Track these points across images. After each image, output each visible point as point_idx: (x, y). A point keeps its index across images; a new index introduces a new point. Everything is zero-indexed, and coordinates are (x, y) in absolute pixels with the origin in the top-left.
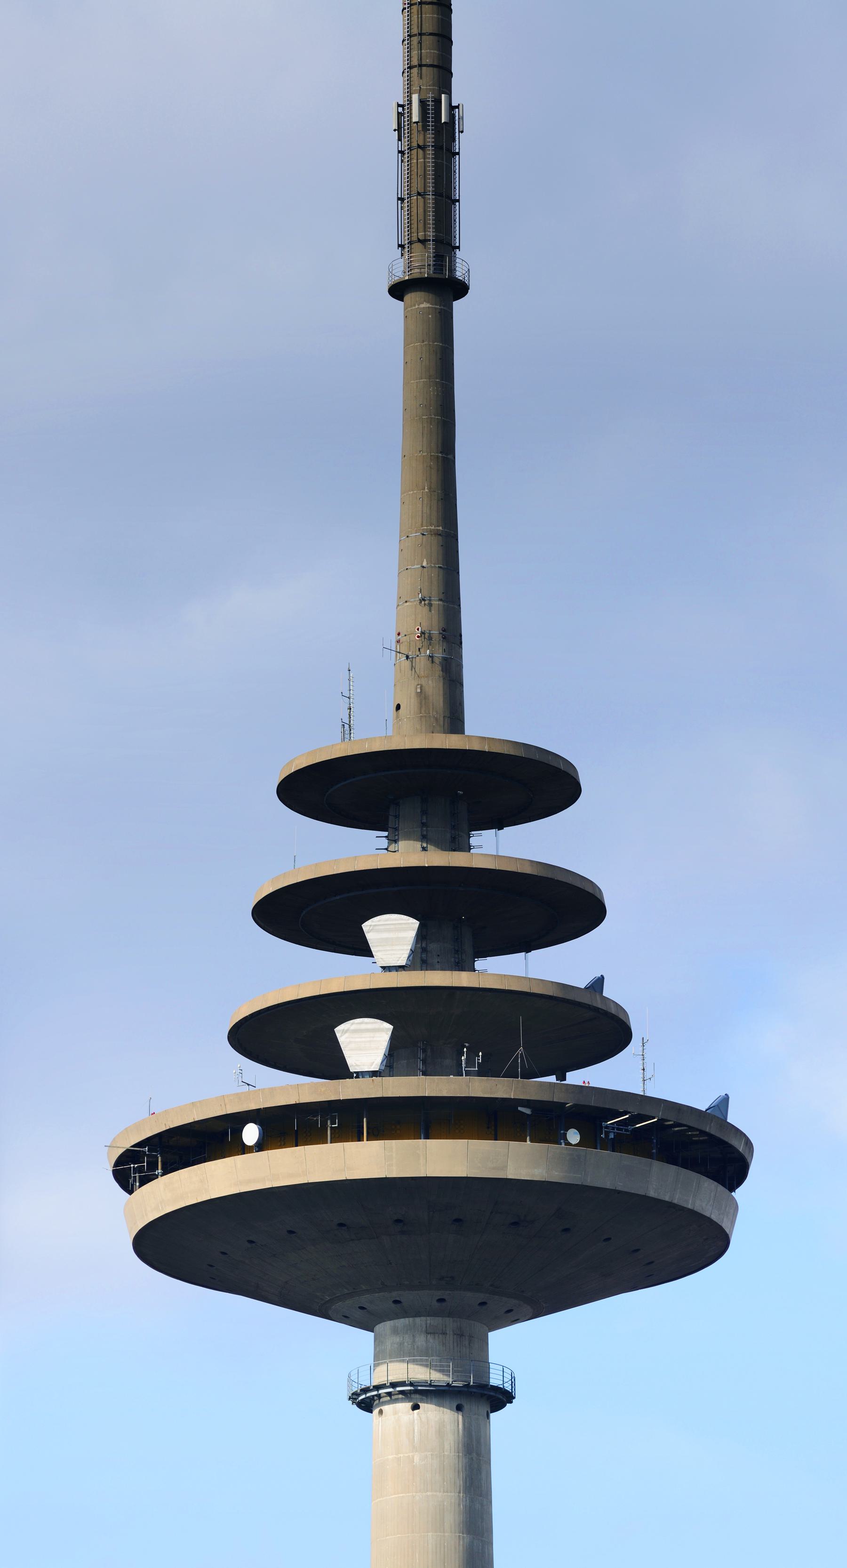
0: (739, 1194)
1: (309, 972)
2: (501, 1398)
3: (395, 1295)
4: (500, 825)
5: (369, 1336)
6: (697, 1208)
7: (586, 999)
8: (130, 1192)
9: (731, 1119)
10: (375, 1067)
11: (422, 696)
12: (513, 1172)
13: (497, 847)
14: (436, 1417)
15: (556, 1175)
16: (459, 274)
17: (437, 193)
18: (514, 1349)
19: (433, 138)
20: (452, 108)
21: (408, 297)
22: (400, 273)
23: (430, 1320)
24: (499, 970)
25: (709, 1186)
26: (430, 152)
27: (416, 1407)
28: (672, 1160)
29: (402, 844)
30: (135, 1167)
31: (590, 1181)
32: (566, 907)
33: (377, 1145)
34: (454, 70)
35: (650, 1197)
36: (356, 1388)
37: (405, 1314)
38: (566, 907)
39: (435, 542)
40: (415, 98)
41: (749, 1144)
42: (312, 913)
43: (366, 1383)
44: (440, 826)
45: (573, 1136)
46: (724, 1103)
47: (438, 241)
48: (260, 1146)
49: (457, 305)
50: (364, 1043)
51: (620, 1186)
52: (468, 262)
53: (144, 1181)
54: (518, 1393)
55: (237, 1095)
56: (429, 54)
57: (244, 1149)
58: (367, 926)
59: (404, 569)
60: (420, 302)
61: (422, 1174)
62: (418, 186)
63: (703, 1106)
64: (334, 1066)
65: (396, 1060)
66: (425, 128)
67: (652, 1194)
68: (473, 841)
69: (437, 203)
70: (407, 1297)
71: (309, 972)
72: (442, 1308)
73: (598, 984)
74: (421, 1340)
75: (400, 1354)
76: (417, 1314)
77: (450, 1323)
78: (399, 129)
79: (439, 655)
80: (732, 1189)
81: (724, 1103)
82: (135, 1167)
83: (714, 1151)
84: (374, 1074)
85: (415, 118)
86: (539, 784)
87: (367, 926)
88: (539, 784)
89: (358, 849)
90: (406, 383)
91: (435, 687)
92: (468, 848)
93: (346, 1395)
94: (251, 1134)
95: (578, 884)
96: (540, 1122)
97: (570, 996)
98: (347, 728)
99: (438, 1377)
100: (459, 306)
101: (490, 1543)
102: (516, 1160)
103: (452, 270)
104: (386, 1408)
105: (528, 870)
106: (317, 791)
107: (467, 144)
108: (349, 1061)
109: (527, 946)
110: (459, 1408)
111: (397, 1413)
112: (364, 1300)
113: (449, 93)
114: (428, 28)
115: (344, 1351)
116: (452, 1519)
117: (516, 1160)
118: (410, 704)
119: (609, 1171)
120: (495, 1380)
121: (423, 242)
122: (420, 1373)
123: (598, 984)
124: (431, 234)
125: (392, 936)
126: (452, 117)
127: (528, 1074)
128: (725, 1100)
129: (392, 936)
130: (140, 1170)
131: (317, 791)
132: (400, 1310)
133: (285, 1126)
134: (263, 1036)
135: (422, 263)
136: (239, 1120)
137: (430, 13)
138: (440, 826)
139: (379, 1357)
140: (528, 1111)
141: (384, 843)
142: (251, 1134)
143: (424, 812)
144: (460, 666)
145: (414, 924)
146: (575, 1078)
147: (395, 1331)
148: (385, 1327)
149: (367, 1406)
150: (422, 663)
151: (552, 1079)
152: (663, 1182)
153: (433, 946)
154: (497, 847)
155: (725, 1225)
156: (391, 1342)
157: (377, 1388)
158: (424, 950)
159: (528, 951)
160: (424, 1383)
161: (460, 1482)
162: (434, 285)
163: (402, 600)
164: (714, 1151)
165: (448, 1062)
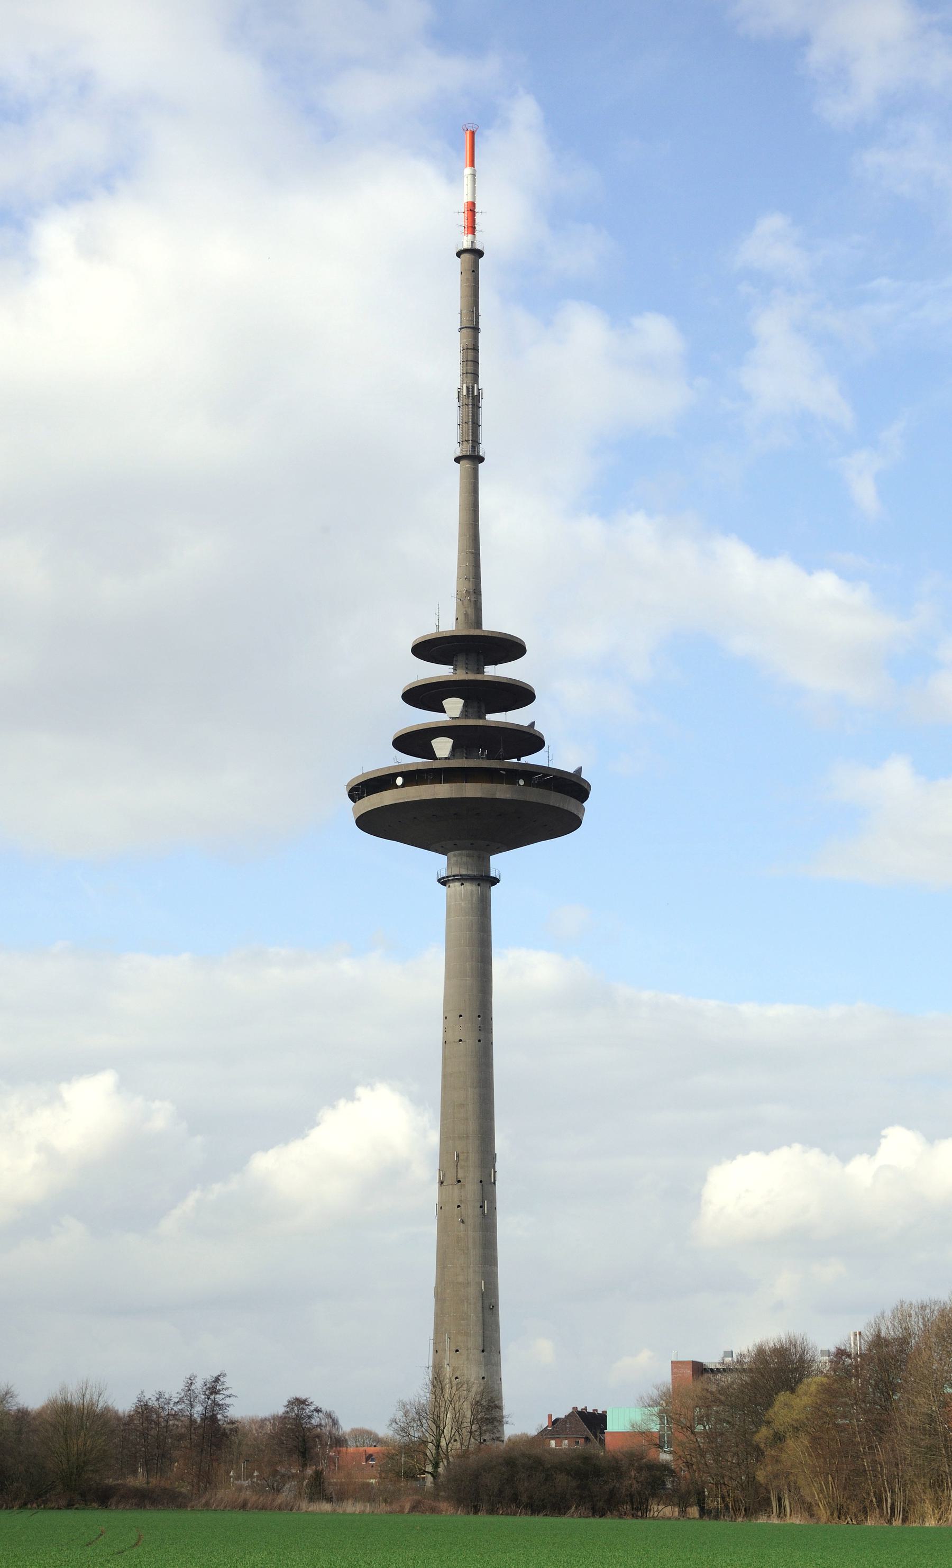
2: (495, 881)
11: (466, 615)
13: (493, 671)
14: (469, 887)
15: (515, 797)
16: (481, 454)
17: (473, 423)
18: (499, 863)
19: (471, 401)
22: (459, 453)
23: (456, 852)
25: (574, 801)
26: (470, 406)
35: (555, 805)
38: (520, 695)
39: (471, 556)
41: (589, 785)
42: (422, 696)
45: (522, 782)
47: (473, 441)
50: (442, 746)
51: (540, 801)
52: (484, 449)
56: (470, 368)
57: (397, 787)
60: (466, 464)
64: (431, 755)
73: (533, 724)
74: (464, 859)
79: (473, 599)
82: (358, 791)
83: (575, 788)
88: (511, 648)
89: (443, 672)
91: (471, 611)
98: (438, 627)
102: (501, 791)
104: (451, 885)
105: (505, 681)
106: (427, 650)
107: (483, 403)
109: (506, 709)
114: (470, 358)
115: (437, 863)
117: (501, 791)
118: (461, 618)
119: (535, 795)
120: (492, 874)
123: (533, 724)
124: (470, 438)
128: (580, 769)
129: (454, 706)
131: (427, 650)
132: (456, 847)
134: (404, 743)
136: (395, 776)
137: (470, 353)
142: (399, 781)
146: (524, 760)
147: (455, 855)
149: (444, 884)
150: (466, 602)
151: (515, 760)
153: (470, 710)
154: (493, 671)
156: (453, 859)
164: (575, 788)
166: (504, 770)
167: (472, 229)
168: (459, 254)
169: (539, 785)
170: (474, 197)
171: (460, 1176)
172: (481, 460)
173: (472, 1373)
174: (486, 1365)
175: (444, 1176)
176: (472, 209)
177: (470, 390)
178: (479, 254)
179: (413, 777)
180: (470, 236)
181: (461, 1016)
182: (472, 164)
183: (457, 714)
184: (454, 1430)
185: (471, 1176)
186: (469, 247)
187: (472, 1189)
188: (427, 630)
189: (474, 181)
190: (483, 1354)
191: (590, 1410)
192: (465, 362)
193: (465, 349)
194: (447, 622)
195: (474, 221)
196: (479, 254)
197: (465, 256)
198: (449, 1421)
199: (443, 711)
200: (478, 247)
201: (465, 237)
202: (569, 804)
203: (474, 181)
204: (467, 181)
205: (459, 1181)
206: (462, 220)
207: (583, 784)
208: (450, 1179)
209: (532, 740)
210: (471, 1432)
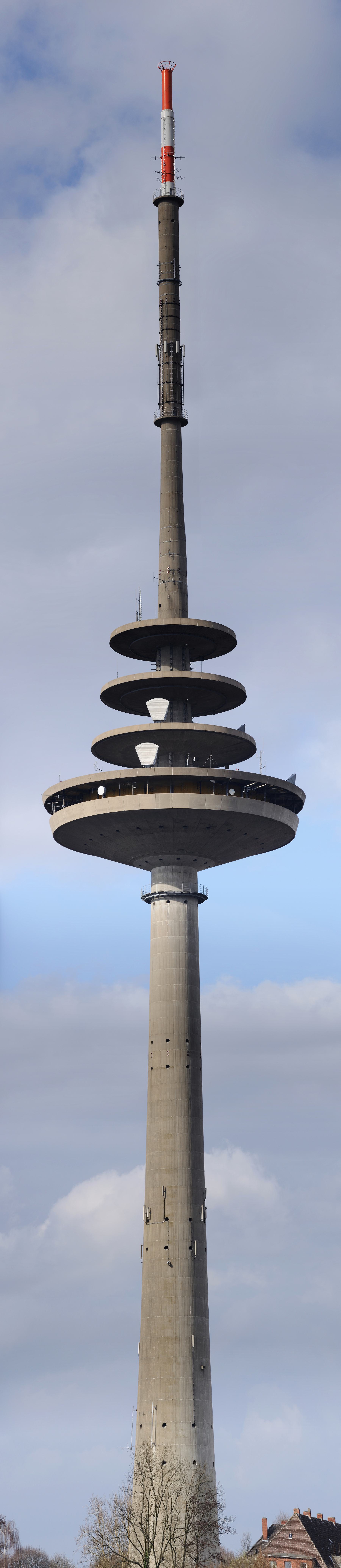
0: (299, 815)
1: (125, 722)
2: (202, 898)
3: (160, 857)
4: (202, 659)
5: (150, 873)
6: (282, 821)
7: (238, 735)
8: (52, 814)
9: (296, 784)
10: (152, 763)
11: (170, 600)
12: (208, 806)
13: (202, 669)
15: (225, 808)
16: (184, 416)
17: (174, 382)
18: (208, 879)
19: (172, 360)
20: (180, 347)
21: (162, 426)
22: (159, 416)
24: (203, 722)
25: (287, 812)
26: (171, 365)
27: (168, 902)
28: (272, 801)
29: (162, 668)
30: (53, 803)
31: (238, 810)
32: (230, 695)
33: (152, 796)
34: (181, 330)
35: (264, 816)
36: (144, 894)
37: (164, 864)
38: (230, 695)
40: (165, 342)
41: (304, 794)
43: (148, 892)
44: (177, 656)
45: (232, 792)
46: (294, 777)
47: (175, 402)
48: (105, 796)
49: (183, 429)
50: (147, 753)
51: (251, 812)
52: (187, 410)
53: (57, 810)
54: (209, 896)
55: (95, 774)
56: (171, 324)
57: (98, 797)
58: (148, 703)
59: (162, 543)
60: (168, 428)
61: (170, 807)
62: (166, 379)
63: (285, 779)
64: (135, 763)
65: (160, 760)
66: (169, 355)
67: (264, 815)
68: (192, 666)
69: (174, 386)
70: (165, 857)
71: (125, 722)
72: (179, 862)
73: (243, 728)
74: (170, 875)
75: (162, 880)
76: (169, 864)
77: (182, 868)
78: (158, 356)
79: (177, 581)
80: (297, 813)
81: (294, 777)
82: (53, 803)
83: (289, 797)
84: (151, 766)
85: (165, 351)
86: (219, 640)
87: (148, 703)
88: (219, 640)
90: (162, 462)
92: (190, 669)
93: (140, 897)
94: (101, 790)
95: (235, 685)
96: (219, 786)
97: (232, 733)
98: (139, 615)
99: (177, 890)
100: (184, 429)
101: (198, 956)
102: (209, 802)
103: (181, 414)
104: (156, 902)
105: (214, 679)
106: (127, 643)
107: (186, 361)
108: (141, 761)
109: (213, 712)
110: (186, 902)
111: (161, 904)
112: (147, 859)
113: (179, 340)
115: (140, 879)
116: (183, 946)
117: (209, 802)
118: (165, 604)
119: (247, 806)
120: (200, 891)
121: (169, 402)
122: (170, 888)
123: (243, 728)
124: (172, 399)
125: (158, 707)
126: (180, 350)
127: (214, 766)
128: (294, 777)
129: (158, 707)
130: (56, 805)
131: (127, 643)
132: (161, 862)
133: (115, 787)
135: (169, 411)
136: (96, 784)
137: (171, 308)
138: (177, 656)
139: (154, 881)
140: (213, 781)
141: (155, 667)
142: (101, 790)
143: (171, 653)
144: (186, 586)
145: (167, 702)
146: (233, 767)
147: (160, 871)
148: (156, 869)
149: (149, 901)
150: (170, 584)
151: (224, 768)
152: (269, 810)
153: (175, 712)
154: (202, 669)
155: (294, 828)
157: (153, 894)
158: (171, 714)
159: (214, 714)
160: (172, 892)
161: (186, 932)
162: (174, 421)
163: (162, 554)
164: (289, 797)
165: (181, 761)
166: (213, 778)
167: (170, 174)
168: (157, 202)
169: (250, 795)
170: (172, 141)
171: (168, 1213)
172: (184, 422)
173: (182, 1453)
174: (198, 1445)
175: (150, 1213)
176: (170, 154)
177: (171, 347)
178: (179, 202)
179: (115, 787)
180: (168, 184)
181: (168, 1040)
182: (170, 106)
183: (162, 716)
184: (166, 1541)
185: (179, 1211)
186: (168, 194)
187: (180, 1228)
188: (127, 622)
189: (172, 124)
190: (193, 1429)
191: (314, 1515)
192: (164, 317)
193: (164, 304)
194: (152, 612)
195: (172, 167)
196: (179, 202)
197: (163, 205)
198: (160, 1528)
199: (146, 713)
200: (178, 194)
201: (163, 185)
202: (282, 815)
203: (172, 124)
204: (164, 125)
205: (167, 1219)
206: (159, 165)
207: (298, 794)
208: (157, 1216)
209: (241, 746)
210: (186, 1545)
